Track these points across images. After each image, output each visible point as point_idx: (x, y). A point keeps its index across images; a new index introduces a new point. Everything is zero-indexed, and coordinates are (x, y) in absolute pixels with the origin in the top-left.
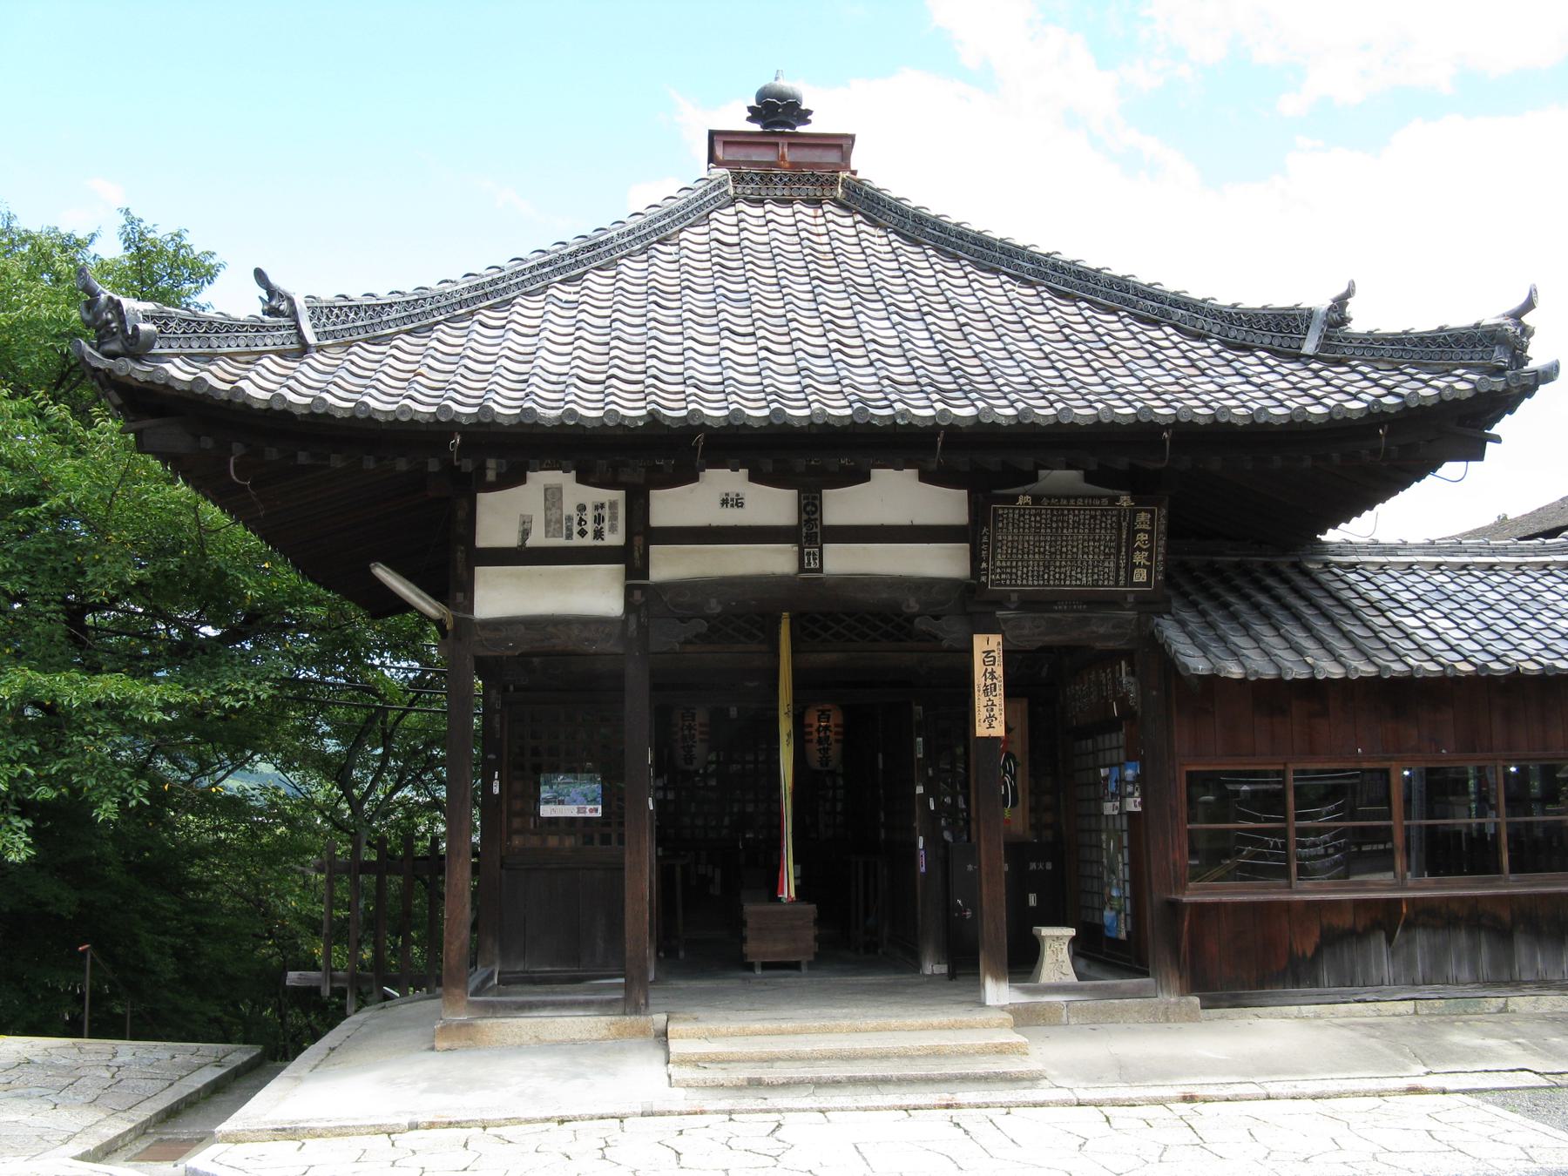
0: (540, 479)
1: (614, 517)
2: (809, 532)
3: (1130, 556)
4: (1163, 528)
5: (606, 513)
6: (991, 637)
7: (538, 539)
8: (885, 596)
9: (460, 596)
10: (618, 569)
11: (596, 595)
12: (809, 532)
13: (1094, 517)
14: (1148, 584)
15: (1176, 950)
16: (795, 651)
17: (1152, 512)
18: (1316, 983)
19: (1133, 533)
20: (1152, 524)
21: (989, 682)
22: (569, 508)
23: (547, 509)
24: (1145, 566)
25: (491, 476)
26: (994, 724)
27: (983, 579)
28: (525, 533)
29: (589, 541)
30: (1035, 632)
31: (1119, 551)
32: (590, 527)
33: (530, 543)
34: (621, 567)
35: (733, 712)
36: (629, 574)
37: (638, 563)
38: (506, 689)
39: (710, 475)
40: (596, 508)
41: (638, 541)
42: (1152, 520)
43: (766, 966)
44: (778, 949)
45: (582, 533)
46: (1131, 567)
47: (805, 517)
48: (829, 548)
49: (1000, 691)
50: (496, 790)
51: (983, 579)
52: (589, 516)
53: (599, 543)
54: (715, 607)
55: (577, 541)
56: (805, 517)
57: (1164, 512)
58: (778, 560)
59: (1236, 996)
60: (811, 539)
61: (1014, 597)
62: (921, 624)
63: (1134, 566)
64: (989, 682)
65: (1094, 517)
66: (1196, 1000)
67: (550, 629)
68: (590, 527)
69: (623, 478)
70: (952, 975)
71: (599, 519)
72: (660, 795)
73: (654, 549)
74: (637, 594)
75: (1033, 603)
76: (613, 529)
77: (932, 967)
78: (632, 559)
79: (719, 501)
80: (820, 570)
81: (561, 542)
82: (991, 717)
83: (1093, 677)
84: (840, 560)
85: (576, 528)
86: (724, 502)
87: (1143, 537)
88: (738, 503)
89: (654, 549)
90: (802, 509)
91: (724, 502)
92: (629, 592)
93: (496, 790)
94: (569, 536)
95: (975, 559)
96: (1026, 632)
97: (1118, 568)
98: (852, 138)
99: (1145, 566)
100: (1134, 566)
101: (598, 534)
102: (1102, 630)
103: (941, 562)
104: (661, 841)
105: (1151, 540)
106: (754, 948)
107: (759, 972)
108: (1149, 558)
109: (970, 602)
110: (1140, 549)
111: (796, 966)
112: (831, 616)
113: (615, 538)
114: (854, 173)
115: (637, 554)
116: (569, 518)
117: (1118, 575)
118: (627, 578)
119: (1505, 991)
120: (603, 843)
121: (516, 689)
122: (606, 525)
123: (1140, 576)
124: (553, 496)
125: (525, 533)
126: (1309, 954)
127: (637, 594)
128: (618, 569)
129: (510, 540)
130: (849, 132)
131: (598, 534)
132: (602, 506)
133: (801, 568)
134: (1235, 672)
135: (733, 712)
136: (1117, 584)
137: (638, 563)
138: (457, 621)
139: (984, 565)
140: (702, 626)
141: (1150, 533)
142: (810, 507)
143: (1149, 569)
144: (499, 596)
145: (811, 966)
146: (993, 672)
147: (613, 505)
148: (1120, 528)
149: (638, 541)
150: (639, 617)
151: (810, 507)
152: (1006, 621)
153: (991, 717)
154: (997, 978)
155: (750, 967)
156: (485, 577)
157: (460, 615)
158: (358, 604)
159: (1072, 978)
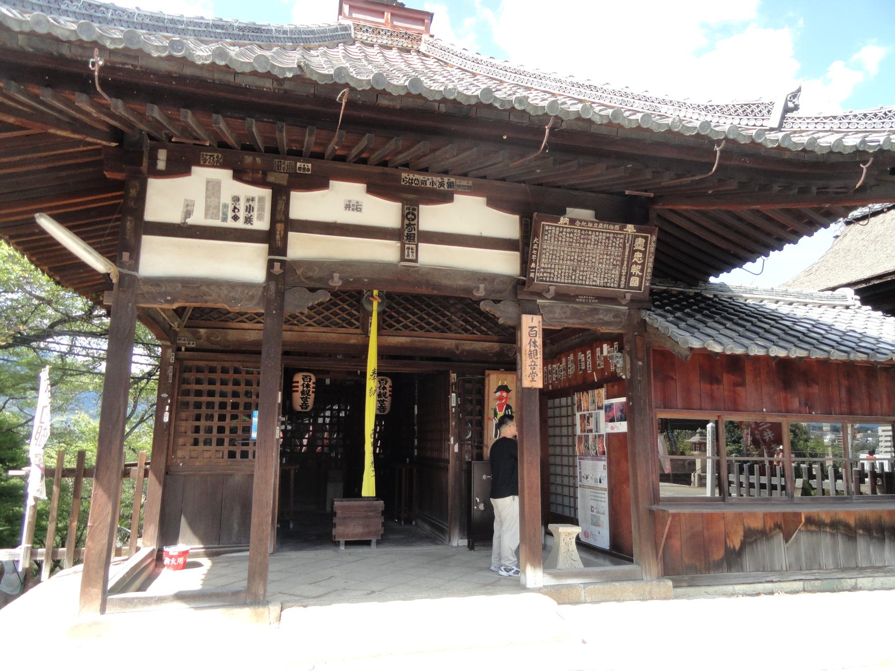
0: (201, 175)
1: (261, 209)
2: (408, 234)
3: (629, 268)
4: (652, 250)
5: (256, 205)
6: (534, 316)
7: (198, 218)
8: (461, 283)
9: (126, 256)
10: (264, 247)
11: (246, 265)
12: (408, 234)
13: (608, 238)
14: (639, 288)
15: (656, 545)
16: (379, 334)
17: (646, 238)
18: (741, 569)
19: (633, 252)
20: (645, 247)
21: (533, 348)
22: (226, 198)
23: (207, 197)
24: (638, 276)
25: (161, 165)
26: (535, 379)
27: (532, 275)
28: (188, 214)
29: (240, 224)
30: (564, 317)
31: (622, 264)
32: (242, 214)
33: (190, 221)
34: (266, 246)
35: (328, 381)
36: (271, 252)
37: (279, 244)
38: (179, 349)
39: (337, 186)
40: (248, 200)
41: (280, 227)
42: (646, 243)
43: (348, 544)
44: (355, 530)
45: (235, 218)
46: (629, 275)
47: (406, 222)
48: (422, 246)
49: (540, 355)
50: (166, 419)
51: (532, 275)
52: (242, 206)
53: (248, 227)
54: (336, 282)
55: (230, 224)
56: (406, 222)
57: (654, 238)
58: (385, 252)
59: (692, 579)
60: (410, 237)
61: (552, 289)
62: (484, 306)
63: (631, 275)
64: (533, 348)
65: (608, 238)
66: (670, 583)
67: (204, 288)
68: (242, 214)
69: (271, 178)
70: (471, 547)
71: (249, 209)
72: (283, 427)
73: (292, 235)
74: (277, 265)
75: (562, 296)
76: (260, 217)
77: (458, 541)
78: (274, 240)
79: (343, 206)
80: (416, 261)
81: (217, 223)
82: (533, 374)
83: (571, 357)
84: (430, 256)
85: (230, 214)
86: (348, 207)
87: (638, 255)
88: (357, 208)
89: (292, 235)
90: (404, 216)
91: (348, 207)
92: (270, 264)
93: (166, 419)
94: (225, 219)
95: (525, 263)
96: (556, 315)
97: (621, 275)
98: (431, 15)
99: (638, 276)
100: (631, 275)
101: (248, 220)
102: (606, 319)
103: (504, 264)
104: (282, 454)
105: (644, 258)
106: (339, 531)
107: (342, 548)
108: (642, 270)
109: (521, 290)
110: (636, 263)
111: (367, 543)
112: (417, 300)
113: (262, 224)
114: (432, 36)
115: (278, 237)
116: (225, 206)
117: (620, 278)
118: (270, 253)
119: (854, 574)
120: (242, 457)
121: (187, 350)
122: (255, 214)
123: (635, 282)
124: (213, 188)
125: (188, 214)
126: (737, 548)
127: (277, 265)
128: (264, 247)
129: (174, 217)
130: (430, 11)
131: (248, 220)
132: (253, 199)
133: (403, 259)
134: (718, 349)
135: (328, 381)
136: (619, 287)
137: (279, 244)
138: (122, 277)
139: (533, 265)
140: (324, 297)
141: (644, 253)
142: (410, 216)
143: (641, 278)
144: (159, 259)
145: (378, 543)
146: (535, 342)
147: (261, 199)
148: (624, 248)
149: (280, 227)
150: (277, 285)
151: (410, 216)
152: (544, 307)
153: (533, 374)
154: (534, 566)
155: (337, 544)
156: (150, 244)
157: (125, 271)
158: (76, 290)
159: (579, 565)
